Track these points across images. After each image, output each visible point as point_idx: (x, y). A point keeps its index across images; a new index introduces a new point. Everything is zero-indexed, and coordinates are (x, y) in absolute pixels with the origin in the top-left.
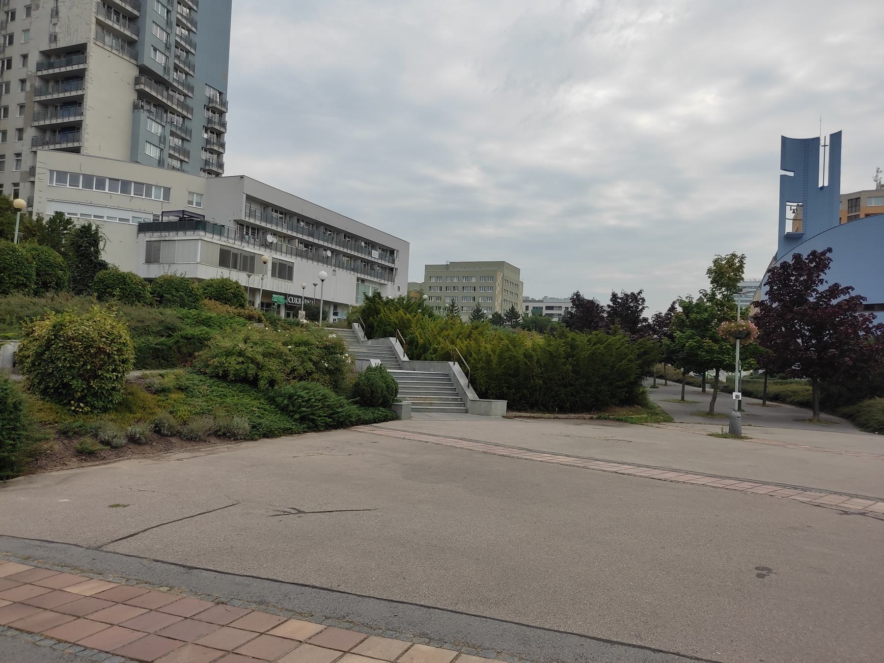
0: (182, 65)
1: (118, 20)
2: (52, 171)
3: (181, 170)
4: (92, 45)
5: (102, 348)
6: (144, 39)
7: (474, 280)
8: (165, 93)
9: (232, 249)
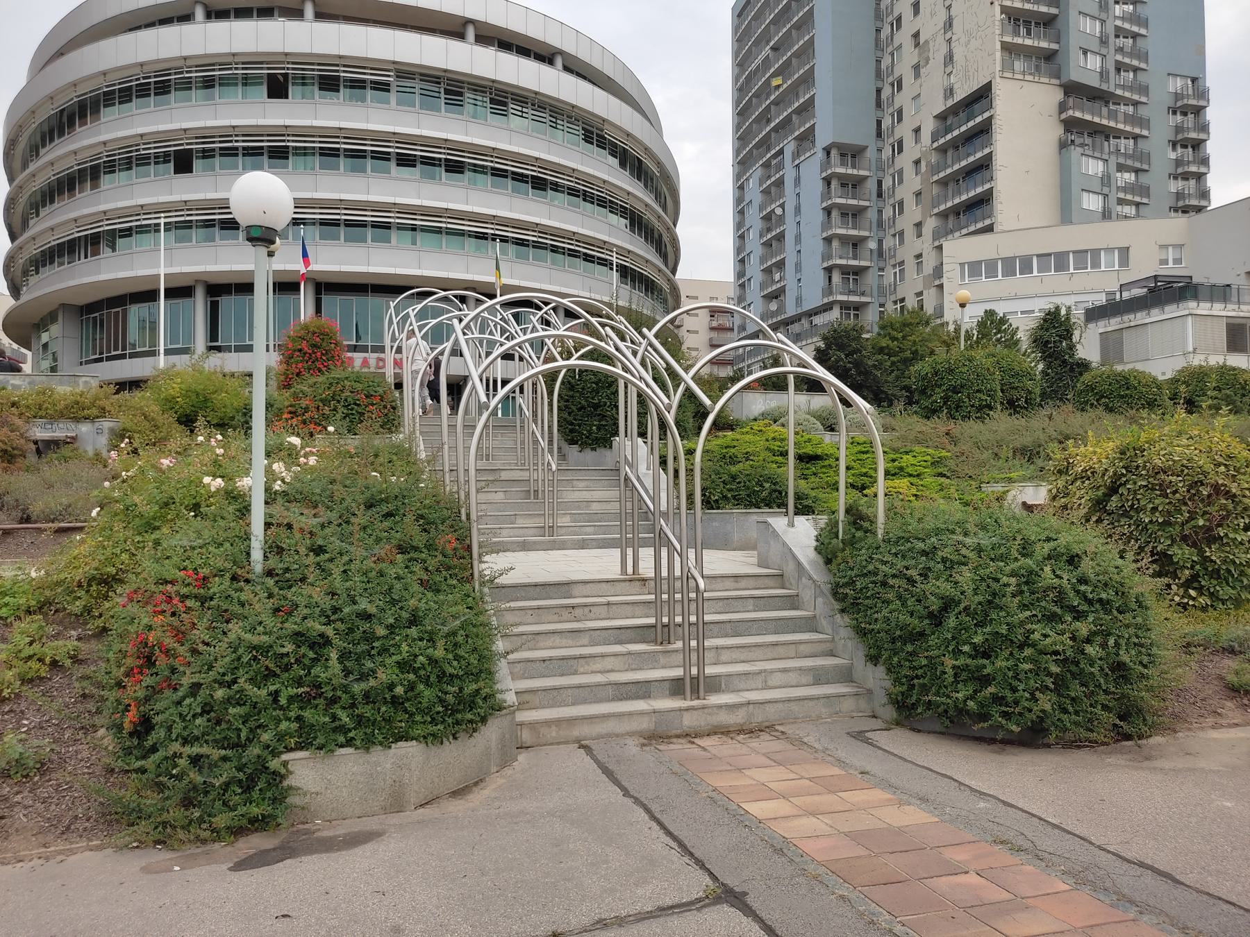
0: (1127, 60)
1: (1029, 33)
2: (962, 265)
3: (1138, 216)
4: (998, 79)
5: (1222, 485)
8: (1105, 110)
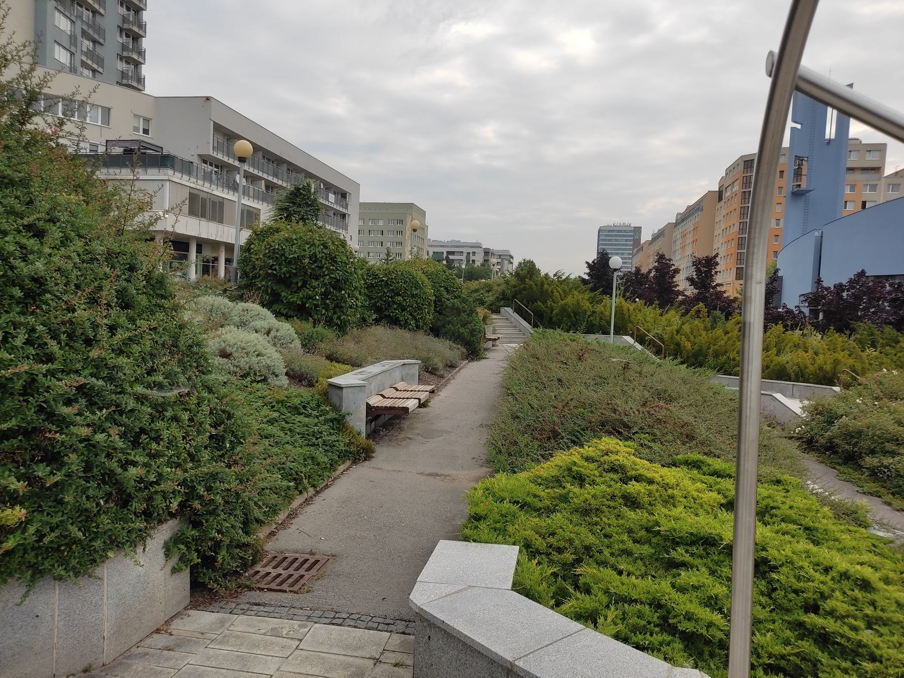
7: (381, 223)
9: (201, 193)
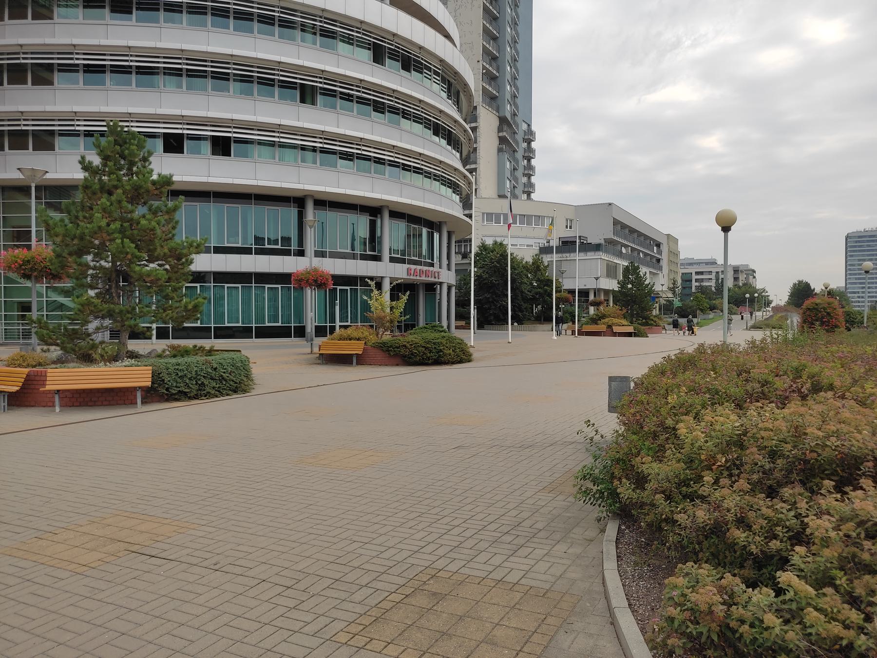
2: (483, 214)
6: (505, 94)
